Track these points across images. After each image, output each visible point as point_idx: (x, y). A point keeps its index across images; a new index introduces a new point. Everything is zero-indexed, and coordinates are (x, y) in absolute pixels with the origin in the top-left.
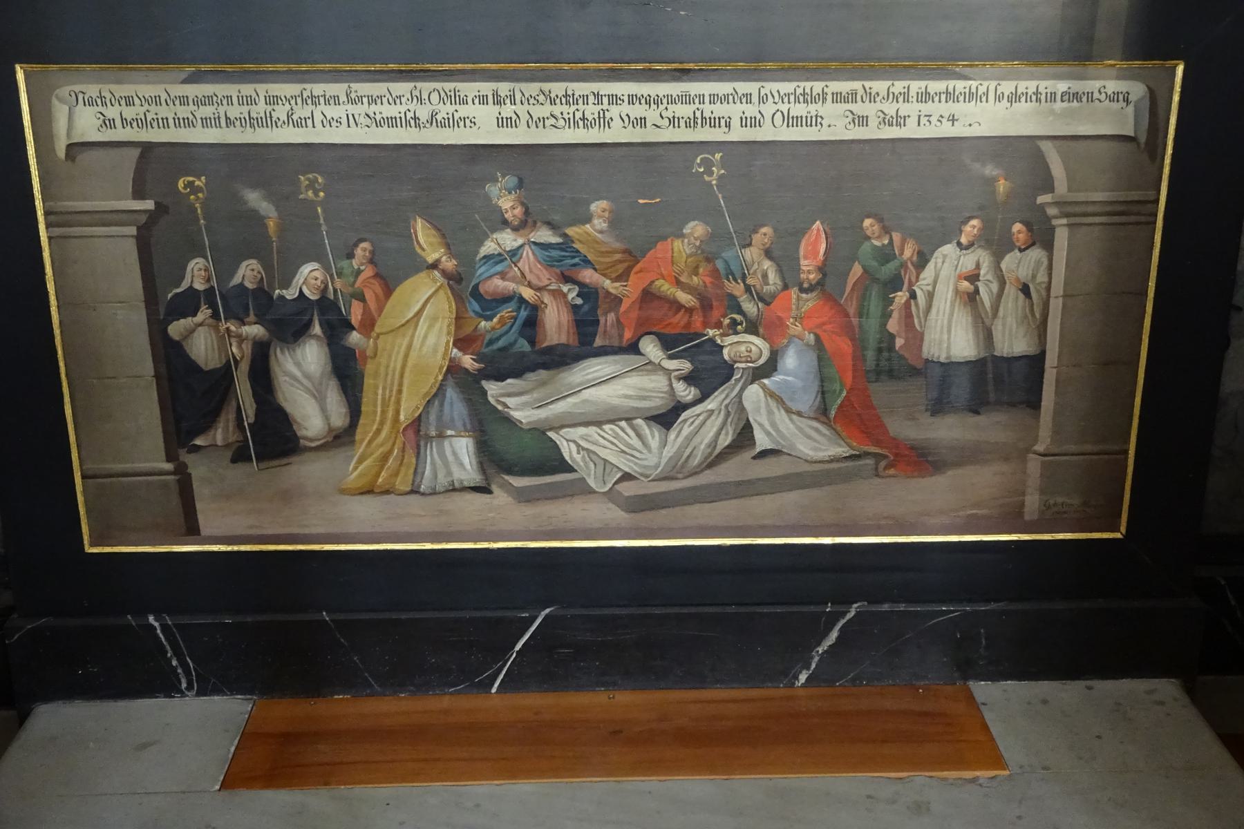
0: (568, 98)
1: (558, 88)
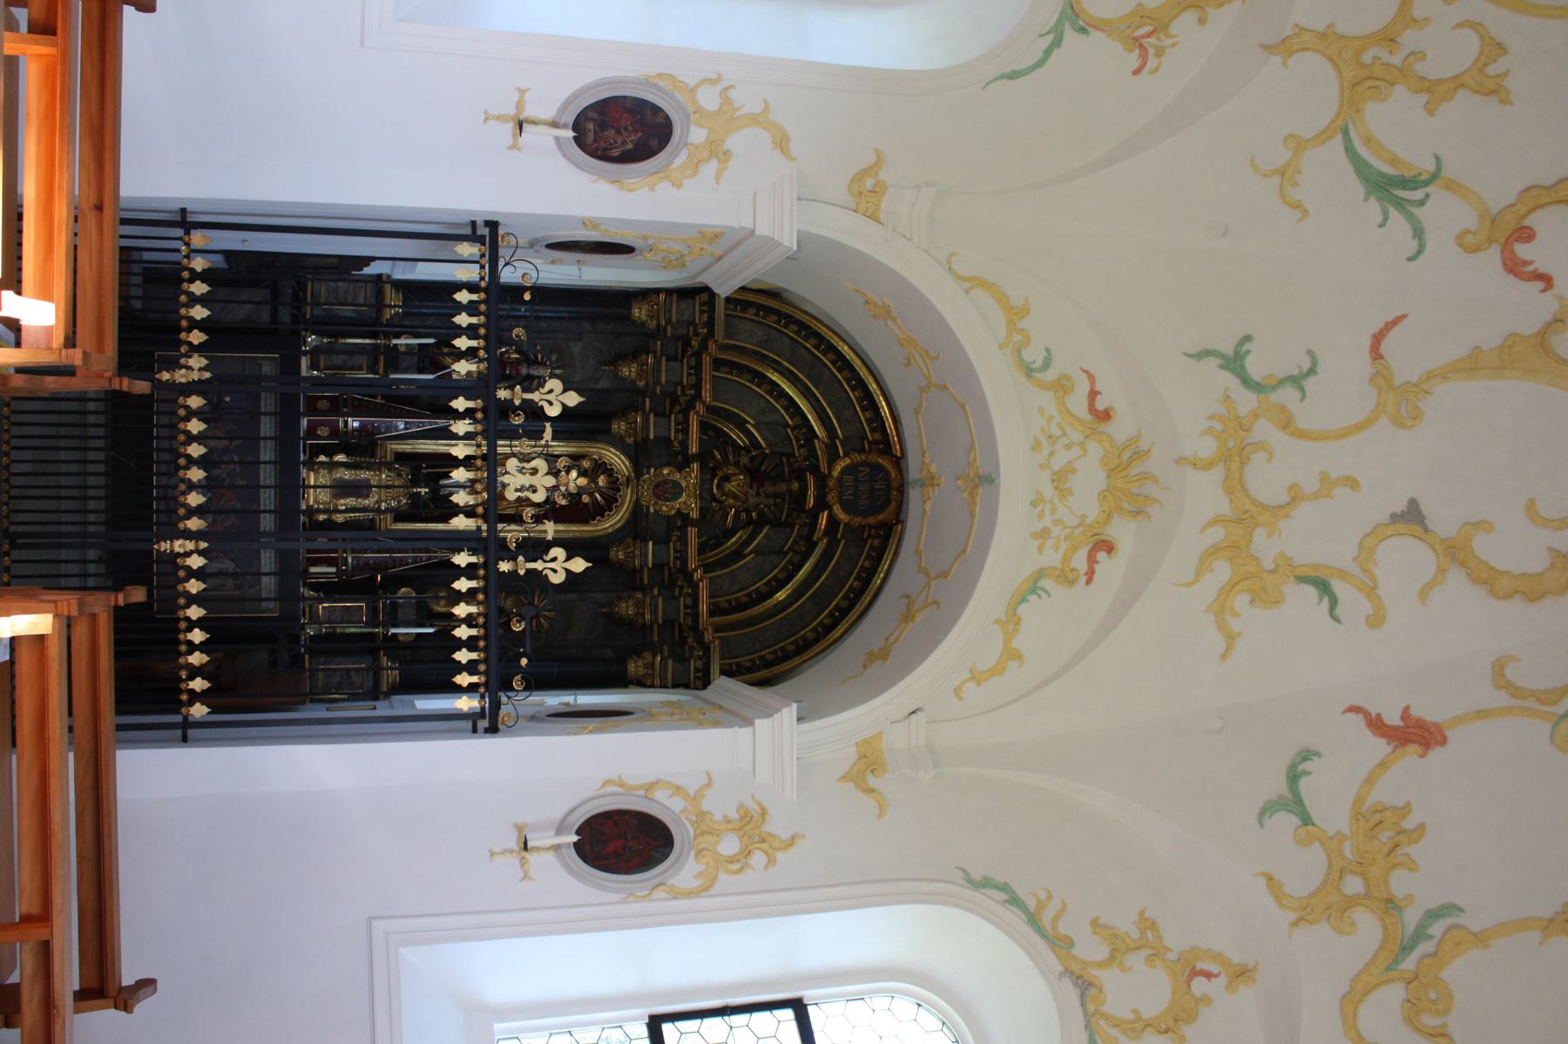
0: (271, 476)
1: (273, 474)
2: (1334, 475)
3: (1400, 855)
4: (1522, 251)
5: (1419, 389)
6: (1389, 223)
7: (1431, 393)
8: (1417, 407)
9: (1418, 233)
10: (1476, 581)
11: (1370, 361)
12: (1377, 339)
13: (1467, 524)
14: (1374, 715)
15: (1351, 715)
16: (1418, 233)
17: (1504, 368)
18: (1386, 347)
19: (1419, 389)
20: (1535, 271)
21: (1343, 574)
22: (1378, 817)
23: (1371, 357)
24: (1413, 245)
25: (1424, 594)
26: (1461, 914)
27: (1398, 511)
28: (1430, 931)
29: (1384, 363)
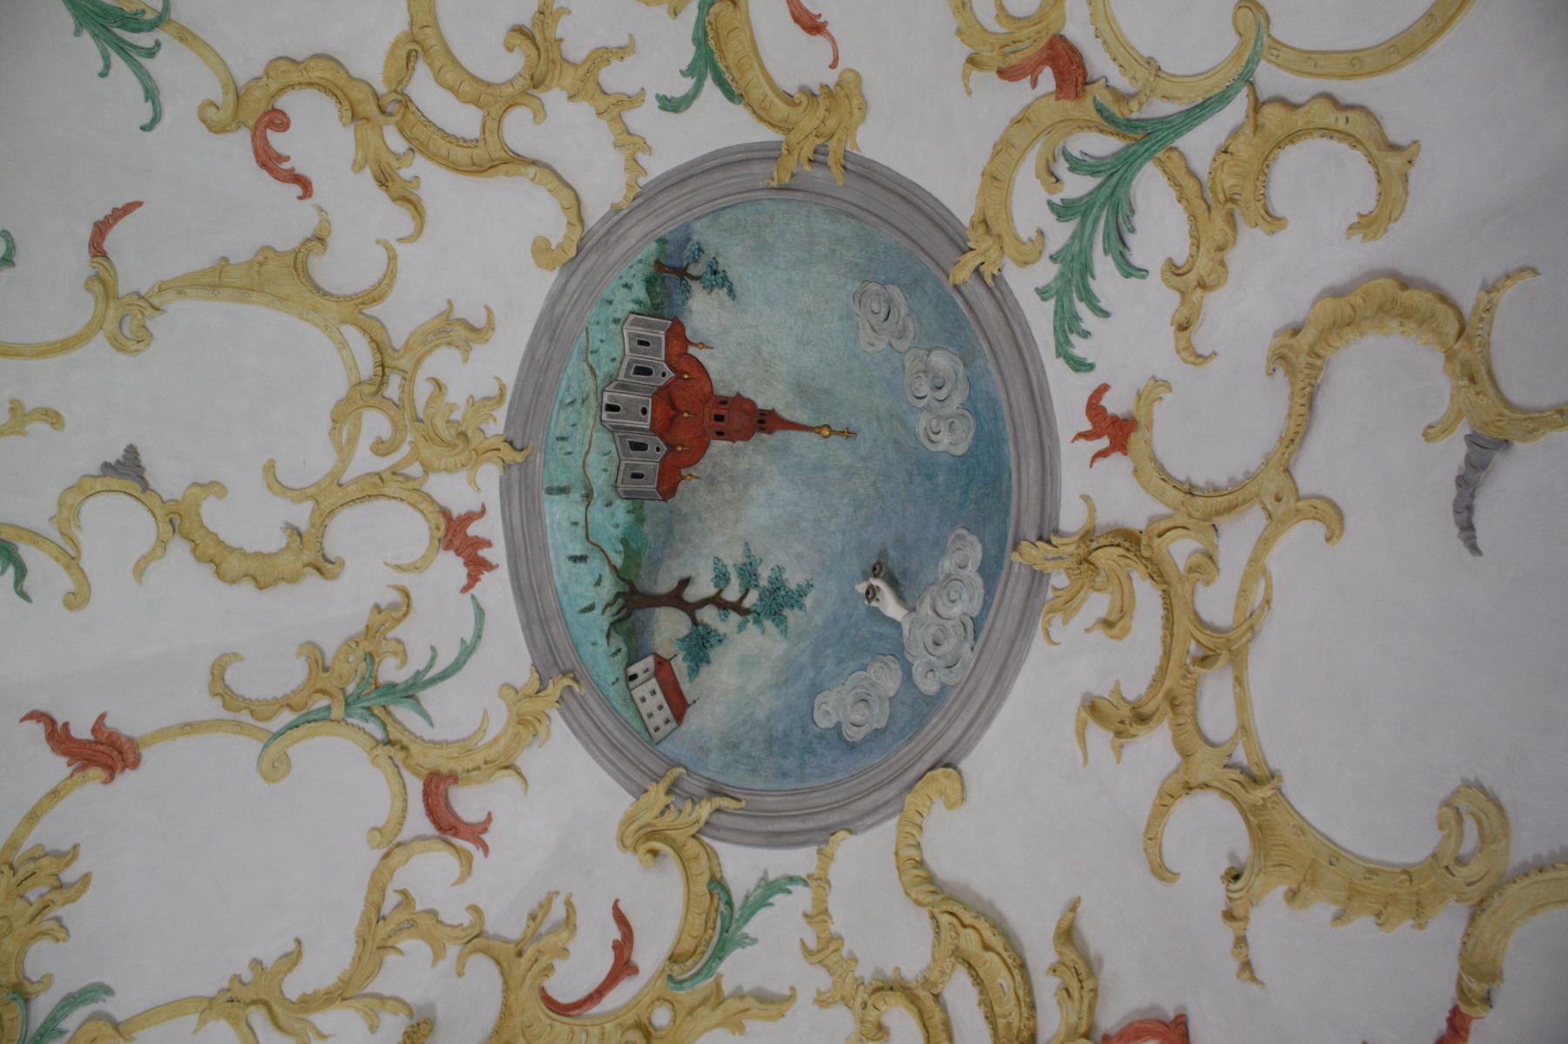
2: (30, 404)
3: (49, 919)
4: (277, 140)
5: (149, 303)
6: (112, 72)
7: (163, 311)
8: (144, 327)
9: (151, 94)
10: (201, 558)
11: (89, 258)
12: (101, 230)
13: (195, 484)
14: (60, 724)
15: (32, 724)
16: (151, 94)
17: (253, 290)
18: (110, 243)
19: (149, 303)
20: (292, 170)
21: (35, 537)
22: (31, 866)
23: (90, 252)
24: (146, 112)
25: (140, 570)
26: (108, 998)
27: (112, 460)
28: (64, 1025)
29: (105, 264)
